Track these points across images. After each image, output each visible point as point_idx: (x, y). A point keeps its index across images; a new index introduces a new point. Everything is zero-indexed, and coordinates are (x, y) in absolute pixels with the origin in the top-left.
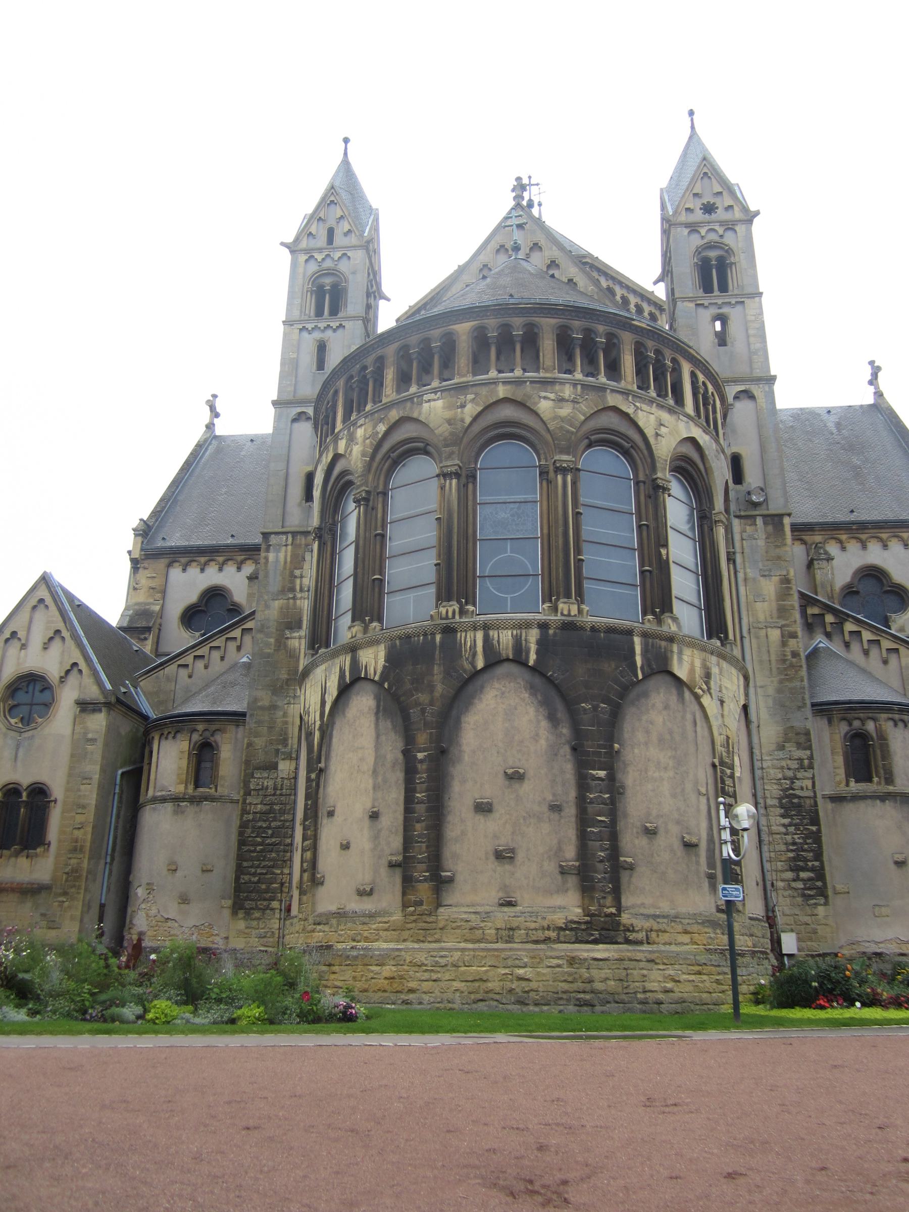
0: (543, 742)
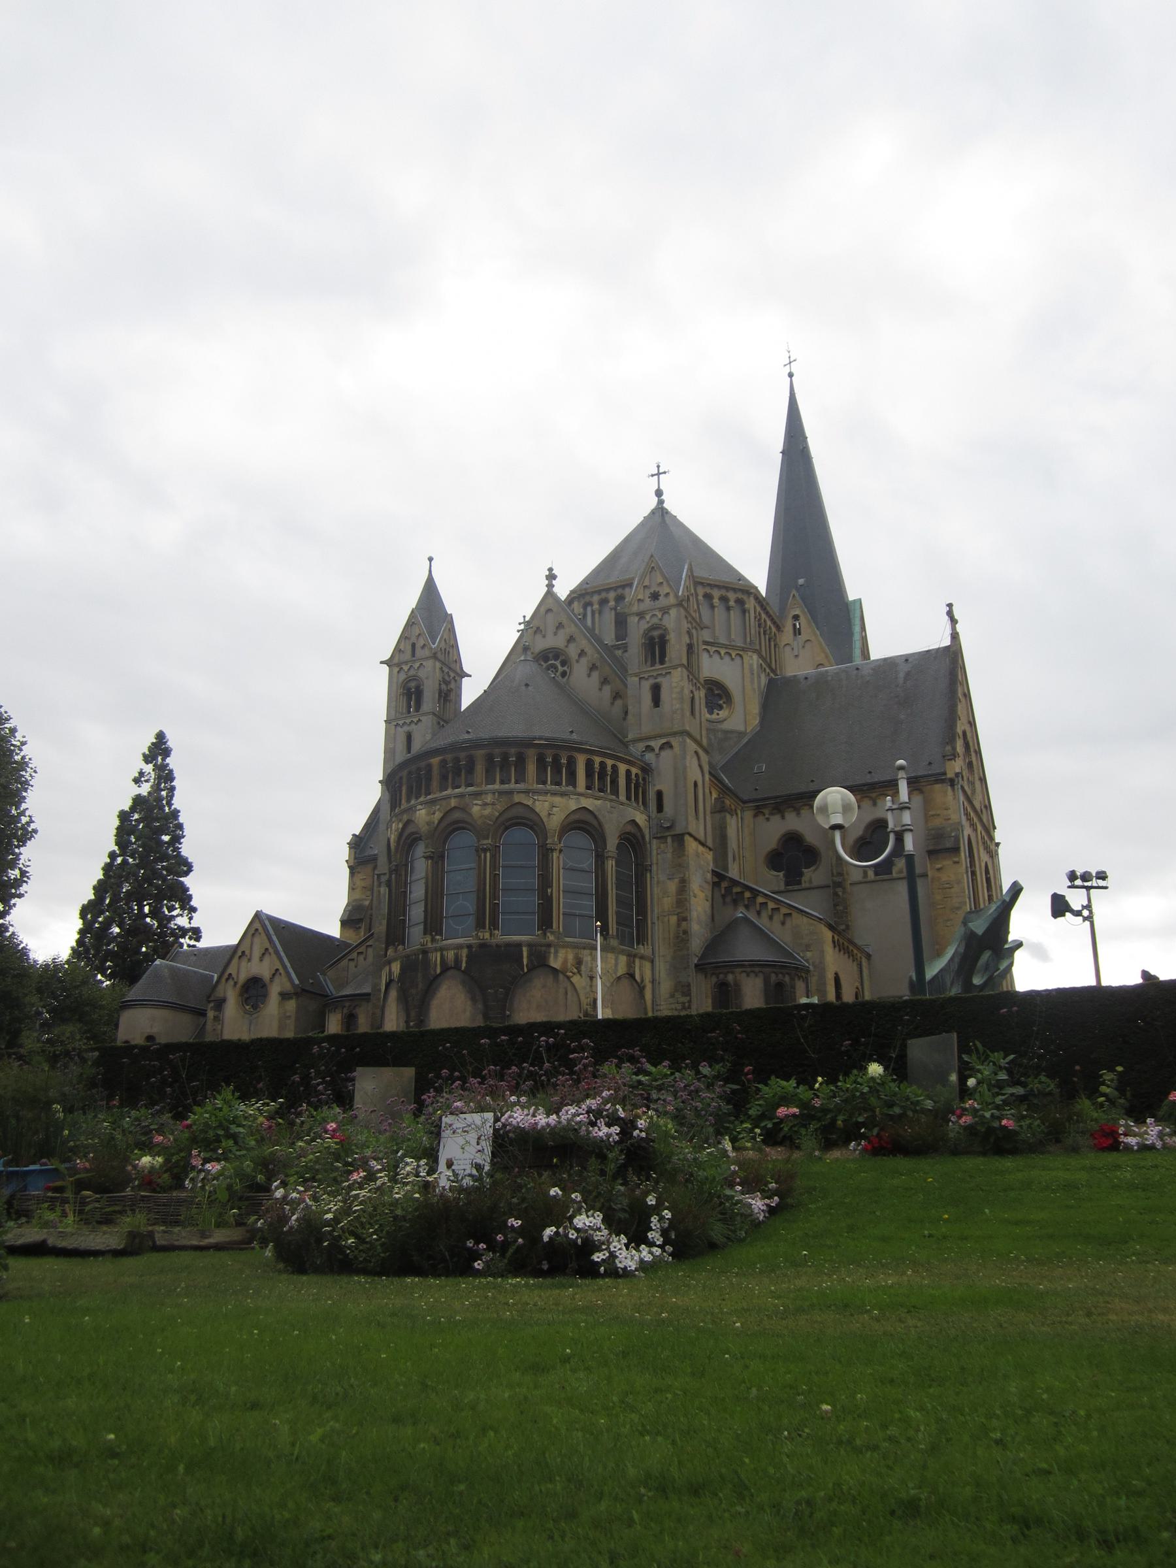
0: (468, 1014)
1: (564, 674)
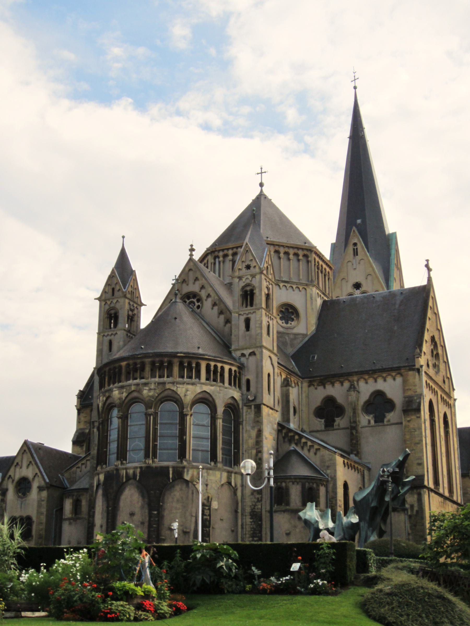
0: (140, 504)
1: (198, 307)
